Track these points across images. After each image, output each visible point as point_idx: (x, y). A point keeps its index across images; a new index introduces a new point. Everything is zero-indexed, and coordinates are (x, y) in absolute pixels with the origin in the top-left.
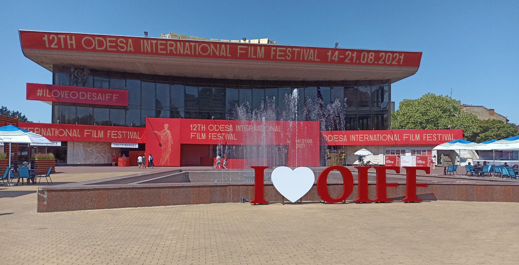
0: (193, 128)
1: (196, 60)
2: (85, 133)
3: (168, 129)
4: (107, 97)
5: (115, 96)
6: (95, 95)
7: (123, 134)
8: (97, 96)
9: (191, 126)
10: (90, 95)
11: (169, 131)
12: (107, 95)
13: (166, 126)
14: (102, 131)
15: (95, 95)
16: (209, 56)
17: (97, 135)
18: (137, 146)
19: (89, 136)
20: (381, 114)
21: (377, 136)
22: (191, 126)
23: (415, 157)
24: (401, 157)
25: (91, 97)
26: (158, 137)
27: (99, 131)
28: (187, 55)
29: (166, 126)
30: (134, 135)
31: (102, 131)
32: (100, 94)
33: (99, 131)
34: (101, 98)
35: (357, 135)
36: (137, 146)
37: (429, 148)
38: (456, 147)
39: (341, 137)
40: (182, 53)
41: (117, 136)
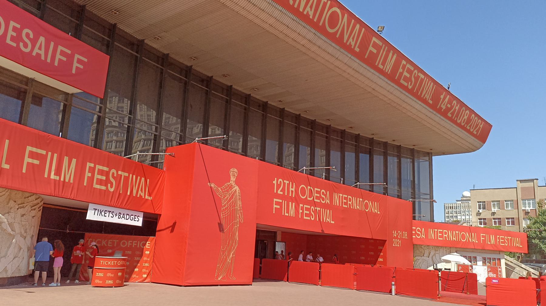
0: (279, 186)
1: (310, 36)
2: (27, 160)
3: (237, 182)
4: (58, 56)
5: (79, 61)
6: (28, 35)
7: (118, 178)
8: (34, 42)
9: (275, 182)
10: (14, 29)
11: (237, 188)
12: (60, 48)
13: (234, 173)
14: (74, 161)
15: (28, 35)
16: (332, 37)
17: (58, 172)
18: (139, 222)
19: (36, 171)
20: (342, 199)
21: (456, 233)
22: (275, 182)
23: (486, 267)
24: (474, 266)
25: (17, 39)
26: (216, 202)
27: (66, 159)
28: (305, 18)
29: (234, 173)
30: (139, 188)
31: (74, 161)
32: (42, 39)
33: (66, 159)
34: (42, 52)
35: (436, 230)
36: (139, 222)
37: (496, 256)
38: (89, 255)
39: (418, 230)
40: (301, 10)
41: (107, 182)
